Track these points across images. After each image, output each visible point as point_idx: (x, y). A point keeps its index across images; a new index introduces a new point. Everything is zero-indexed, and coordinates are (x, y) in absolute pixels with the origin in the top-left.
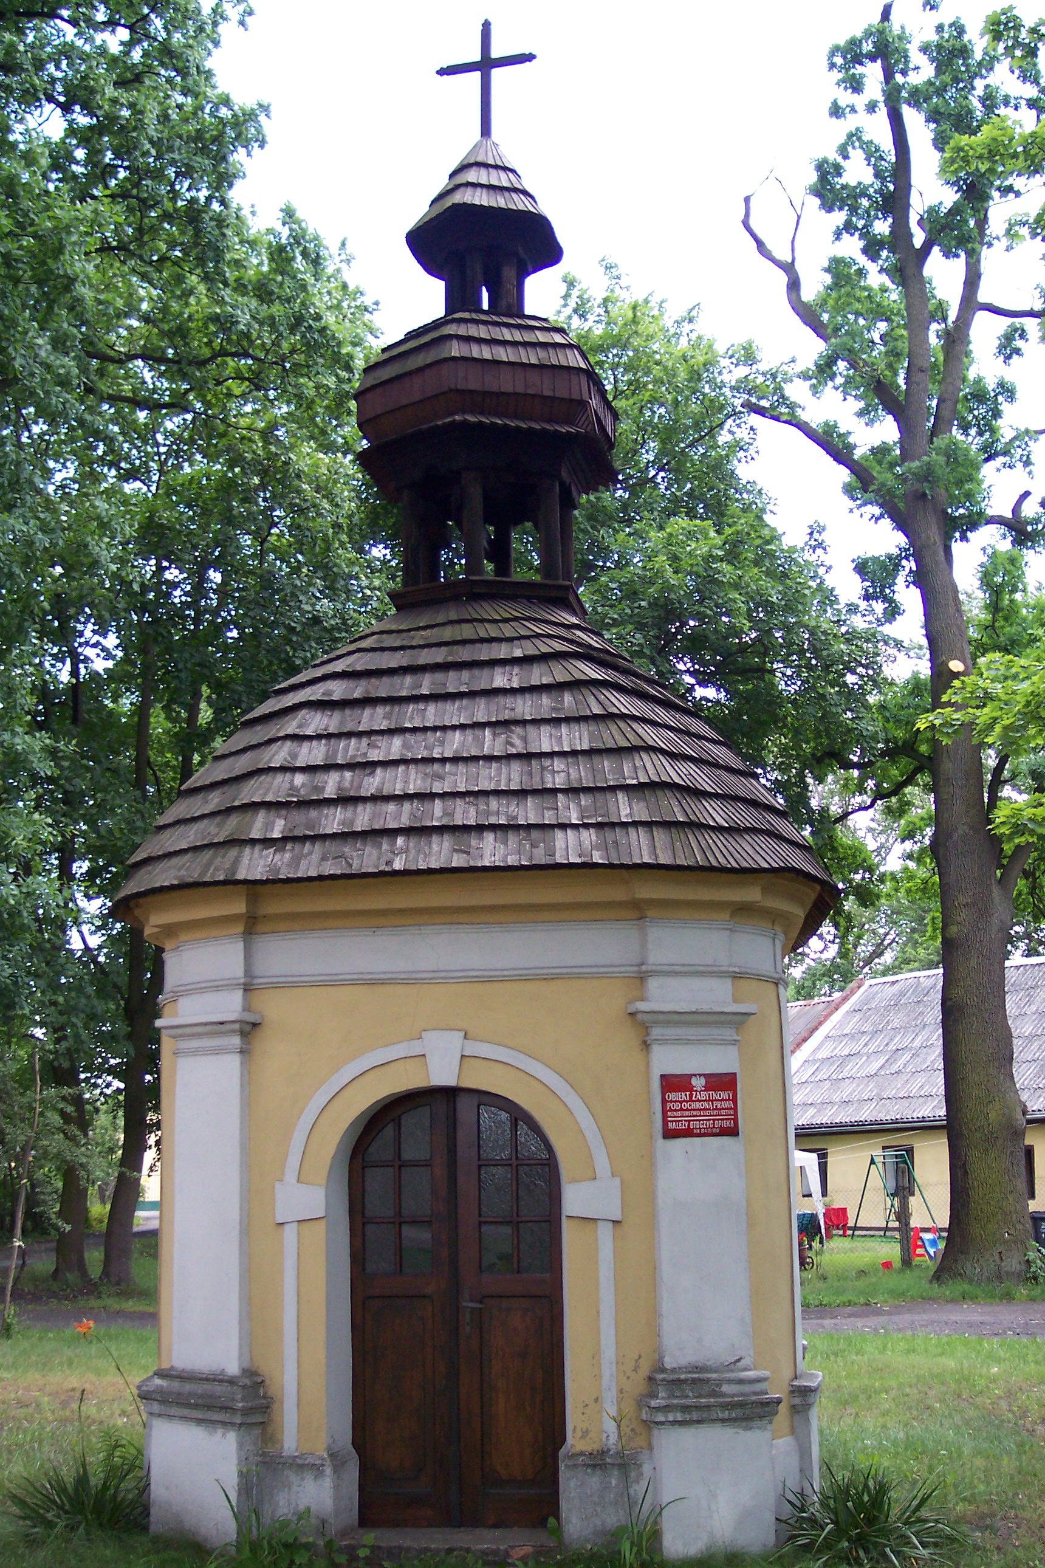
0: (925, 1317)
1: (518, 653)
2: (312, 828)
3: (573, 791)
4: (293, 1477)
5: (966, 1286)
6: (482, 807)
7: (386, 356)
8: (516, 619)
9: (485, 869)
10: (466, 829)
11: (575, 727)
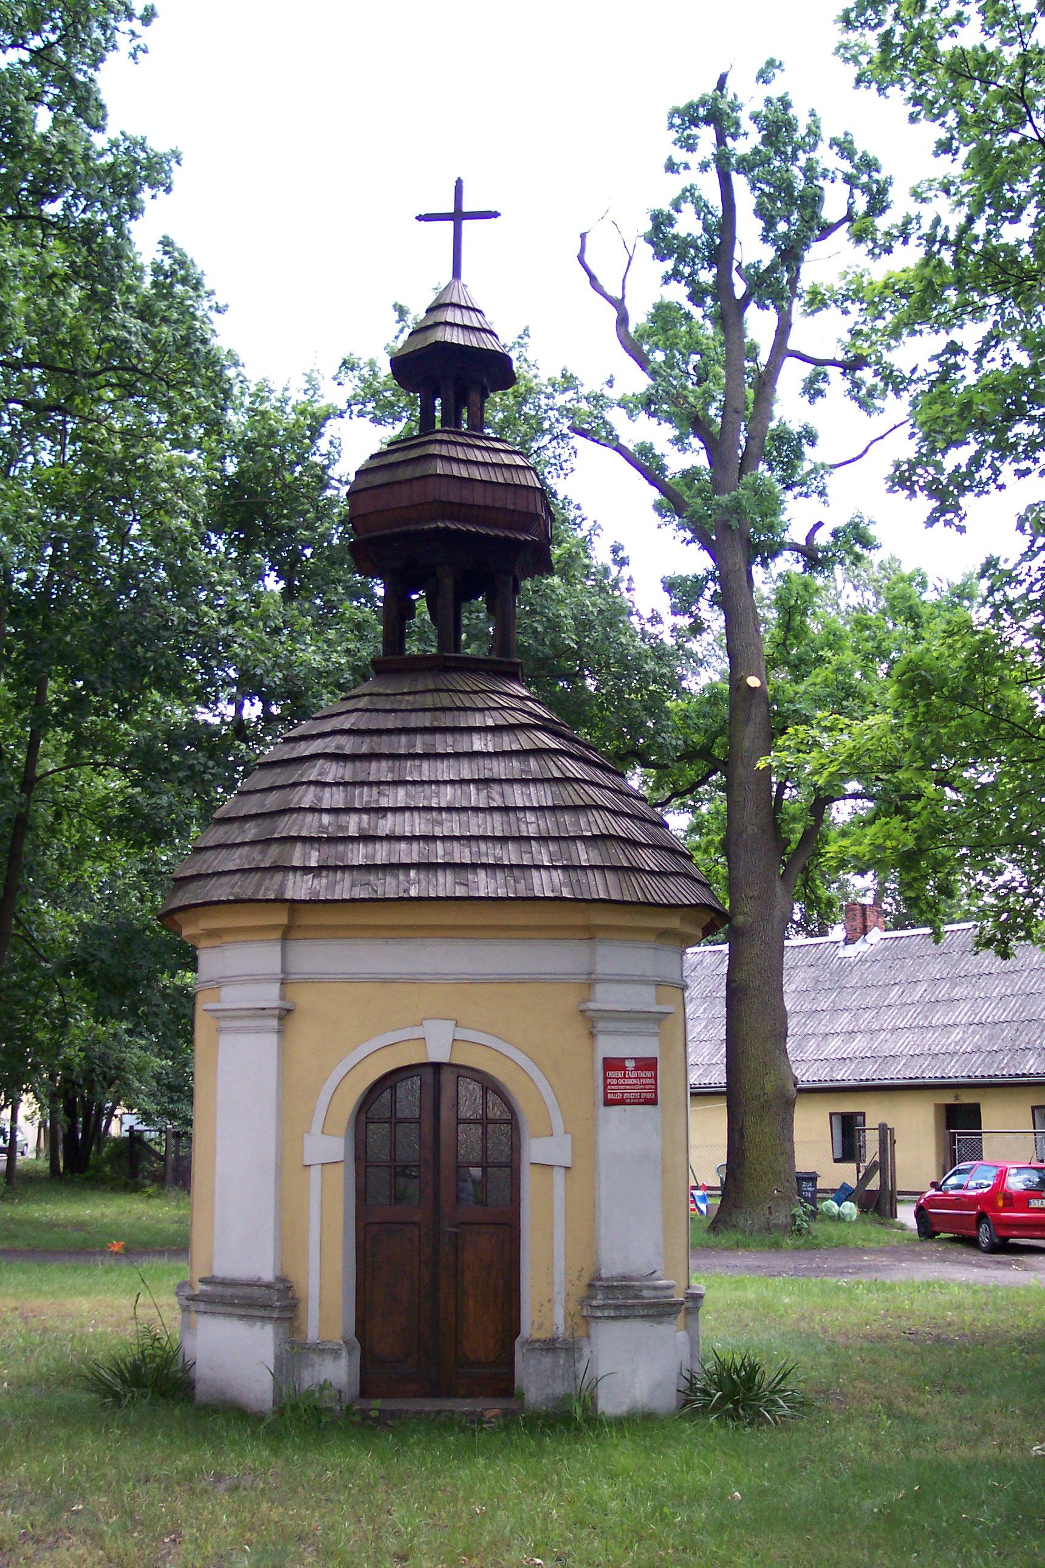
0: (708, 1261)
1: (490, 722)
2: (342, 860)
3: (543, 839)
4: (316, 1359)
5: (740, 1237)
6: (475, 849)
7: (375, 463)
8: (484, 691)
9: (480, 898)
10: (463, 866)
11: (540, 787)
